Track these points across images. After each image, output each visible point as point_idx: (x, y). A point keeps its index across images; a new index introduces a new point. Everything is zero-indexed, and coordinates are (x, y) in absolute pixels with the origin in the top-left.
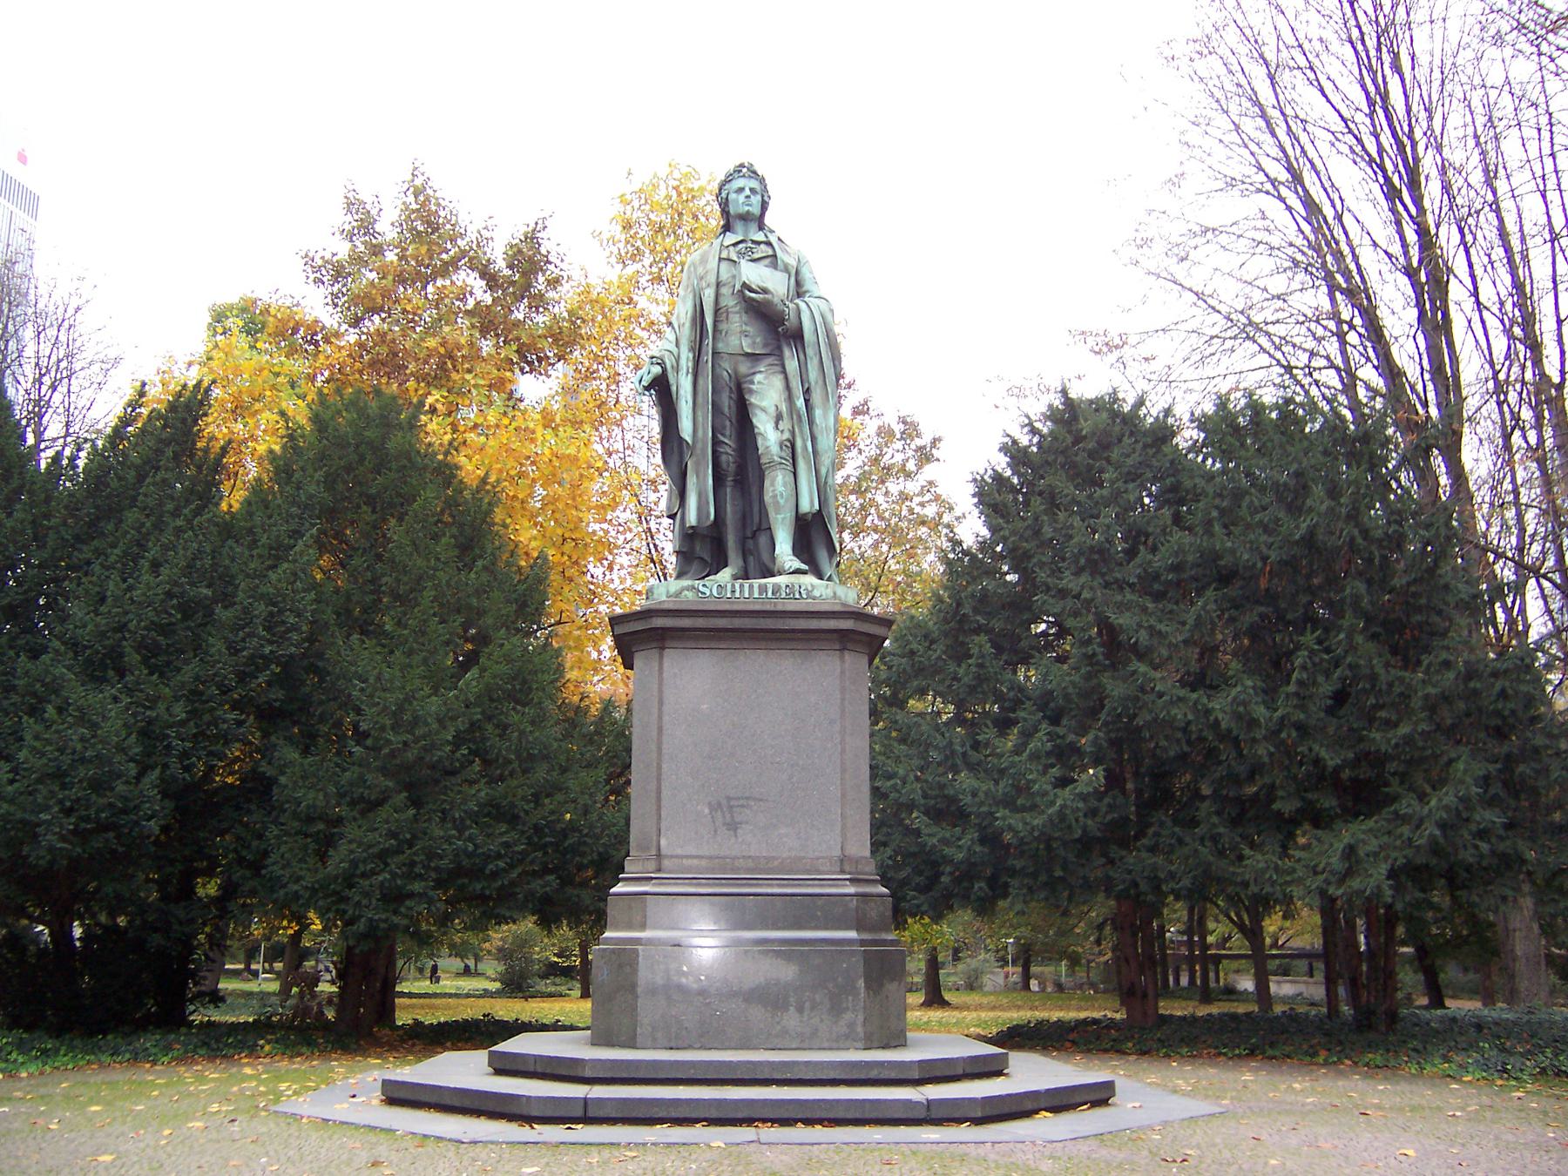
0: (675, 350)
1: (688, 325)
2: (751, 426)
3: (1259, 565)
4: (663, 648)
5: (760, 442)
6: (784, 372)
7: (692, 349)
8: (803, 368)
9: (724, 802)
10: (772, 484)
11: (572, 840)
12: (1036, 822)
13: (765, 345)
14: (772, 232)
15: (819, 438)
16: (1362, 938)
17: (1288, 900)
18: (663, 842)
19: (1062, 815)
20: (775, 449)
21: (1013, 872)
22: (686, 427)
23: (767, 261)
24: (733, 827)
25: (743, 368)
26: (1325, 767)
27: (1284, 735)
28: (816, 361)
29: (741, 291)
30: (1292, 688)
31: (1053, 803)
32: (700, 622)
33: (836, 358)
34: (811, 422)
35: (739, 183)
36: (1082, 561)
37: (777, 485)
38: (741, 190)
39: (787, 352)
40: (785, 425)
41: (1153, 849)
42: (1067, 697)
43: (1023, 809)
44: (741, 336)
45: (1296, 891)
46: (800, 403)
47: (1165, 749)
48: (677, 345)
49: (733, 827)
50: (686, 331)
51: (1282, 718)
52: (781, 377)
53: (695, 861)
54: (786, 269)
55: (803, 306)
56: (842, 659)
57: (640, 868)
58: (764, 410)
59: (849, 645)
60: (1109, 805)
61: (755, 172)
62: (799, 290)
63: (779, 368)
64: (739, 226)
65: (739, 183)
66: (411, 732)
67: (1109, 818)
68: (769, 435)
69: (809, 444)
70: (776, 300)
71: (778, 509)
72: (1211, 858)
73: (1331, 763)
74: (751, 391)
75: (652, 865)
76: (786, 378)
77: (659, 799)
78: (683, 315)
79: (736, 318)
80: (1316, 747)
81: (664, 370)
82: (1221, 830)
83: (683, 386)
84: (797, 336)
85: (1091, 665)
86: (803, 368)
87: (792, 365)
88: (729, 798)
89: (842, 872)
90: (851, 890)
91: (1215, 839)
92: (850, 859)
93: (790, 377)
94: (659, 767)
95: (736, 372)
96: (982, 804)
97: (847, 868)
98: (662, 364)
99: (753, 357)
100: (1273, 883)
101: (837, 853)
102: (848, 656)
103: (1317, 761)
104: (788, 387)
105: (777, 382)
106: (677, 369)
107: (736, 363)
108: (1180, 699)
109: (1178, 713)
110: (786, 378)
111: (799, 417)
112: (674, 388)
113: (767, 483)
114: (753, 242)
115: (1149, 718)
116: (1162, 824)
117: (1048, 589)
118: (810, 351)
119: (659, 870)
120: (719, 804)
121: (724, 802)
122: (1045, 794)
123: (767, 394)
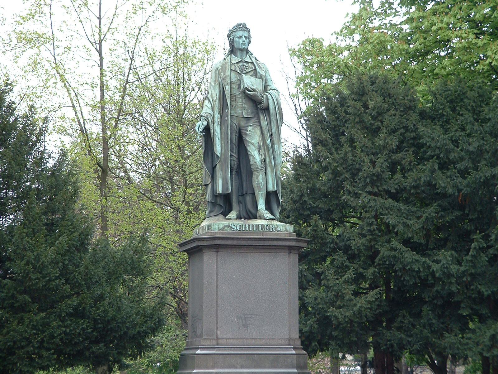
0: (212, 113)
1: (217, 101)
2: (246, 150)
3: (457, 194)
4: (217, 252)
5: (251, 159)
6: (260, 126)
7: (219, 113)
8: (270, 123)
9: (243, 316)
10: (257, 178)
11: (114, 325)
12: (347, 314)
13: (252, 113)
14: (252, 54)
15: (277, 157)
16: (491, 371)
17: (466, 358)
18: (218, 332)
19: (360, 312)
20: (259, 163)
21: (331, 337)
22: (218, 149)
23: (252, 73)
24: (246, 326)
25: (243, 123)
26: (483, 295)
27: (464, 279)
28: (275, 123)
29: (244, 90)
30: (469, 258)
31: (355, 305)
32: (235, 243)
33: (281, 118)
34: (273, 150)
35: (240, 33)
36: (368, 180)
37: (259, 179)
38: (240, 37)
39: (262, 117)
40: (262, 152)
41: (399, 329)
42: (359, 250)
43: (340, 307)
44: (243, 109)
45: (469, 353)
46: (268, 141)
47: (408, 281)
48: (213, 110)
49: (246, 326)
50: (217, 104)
51: (464, 272)
52: (259, 128)
53: (232, 341)
54: (261, 77)
55: (269, 96)
56: (289, 257)
57: (209, 343)
58: (253, 144)
59: (292, 251)
60: (378, 305)
61: (246, 28)
62: (266, 88)
63: (258, 124)
64: (239, 53)
65: (240, 33)
66: (40, 273)
67: (377, 311)
68: (256, 156)
69: (273, 160)
70: (259, 94)
71: (260, 189)
72: (429, 335)
73: (486, 293)
74: (246, 134)
75: (215, 342)
76: (261, 128)
77: (217, 315)
78: (214, 96)
79: (240, 100)
80: (479, 287)
81: (208, 123)
82: (434, 321)
83: (217, 130)
84: (267, 109)
85: (372, 235)
86: (270, 123)
87: (264, 123)
88: (245, 315)
89: (290, 345)
90: (294, 352)
91: (431, 325)
92: (292, 339)
93: (264, 129)
94: (217, 302)
95: (239, 125)
96: (319, 304)
97: (291, 343)
98: (207, 120)
99: (248, 119)
100: (458, 349)
101: (287, 337)
102: (292, 255)
103: (479, 292)
104: (262, 133)
105: (258, 131)
106: (213, 122)
107: (239, 121)
108: (417, 261)
109: (415, 267)
110: (261, 128)
111: (268, 148)
112: (212, 134)
113: (254, 177)
114: (246, 62)
115: (401, 266)
116: (404, 316)
117: (350, 192)
118: (273, 118)
119: (218, 344)
120: (241, 317)
121: (243, 316)
122: (351, 300)
123: (253, 138)
